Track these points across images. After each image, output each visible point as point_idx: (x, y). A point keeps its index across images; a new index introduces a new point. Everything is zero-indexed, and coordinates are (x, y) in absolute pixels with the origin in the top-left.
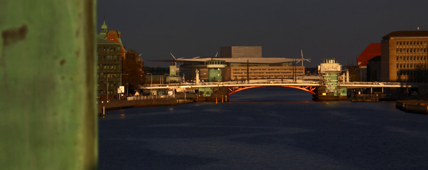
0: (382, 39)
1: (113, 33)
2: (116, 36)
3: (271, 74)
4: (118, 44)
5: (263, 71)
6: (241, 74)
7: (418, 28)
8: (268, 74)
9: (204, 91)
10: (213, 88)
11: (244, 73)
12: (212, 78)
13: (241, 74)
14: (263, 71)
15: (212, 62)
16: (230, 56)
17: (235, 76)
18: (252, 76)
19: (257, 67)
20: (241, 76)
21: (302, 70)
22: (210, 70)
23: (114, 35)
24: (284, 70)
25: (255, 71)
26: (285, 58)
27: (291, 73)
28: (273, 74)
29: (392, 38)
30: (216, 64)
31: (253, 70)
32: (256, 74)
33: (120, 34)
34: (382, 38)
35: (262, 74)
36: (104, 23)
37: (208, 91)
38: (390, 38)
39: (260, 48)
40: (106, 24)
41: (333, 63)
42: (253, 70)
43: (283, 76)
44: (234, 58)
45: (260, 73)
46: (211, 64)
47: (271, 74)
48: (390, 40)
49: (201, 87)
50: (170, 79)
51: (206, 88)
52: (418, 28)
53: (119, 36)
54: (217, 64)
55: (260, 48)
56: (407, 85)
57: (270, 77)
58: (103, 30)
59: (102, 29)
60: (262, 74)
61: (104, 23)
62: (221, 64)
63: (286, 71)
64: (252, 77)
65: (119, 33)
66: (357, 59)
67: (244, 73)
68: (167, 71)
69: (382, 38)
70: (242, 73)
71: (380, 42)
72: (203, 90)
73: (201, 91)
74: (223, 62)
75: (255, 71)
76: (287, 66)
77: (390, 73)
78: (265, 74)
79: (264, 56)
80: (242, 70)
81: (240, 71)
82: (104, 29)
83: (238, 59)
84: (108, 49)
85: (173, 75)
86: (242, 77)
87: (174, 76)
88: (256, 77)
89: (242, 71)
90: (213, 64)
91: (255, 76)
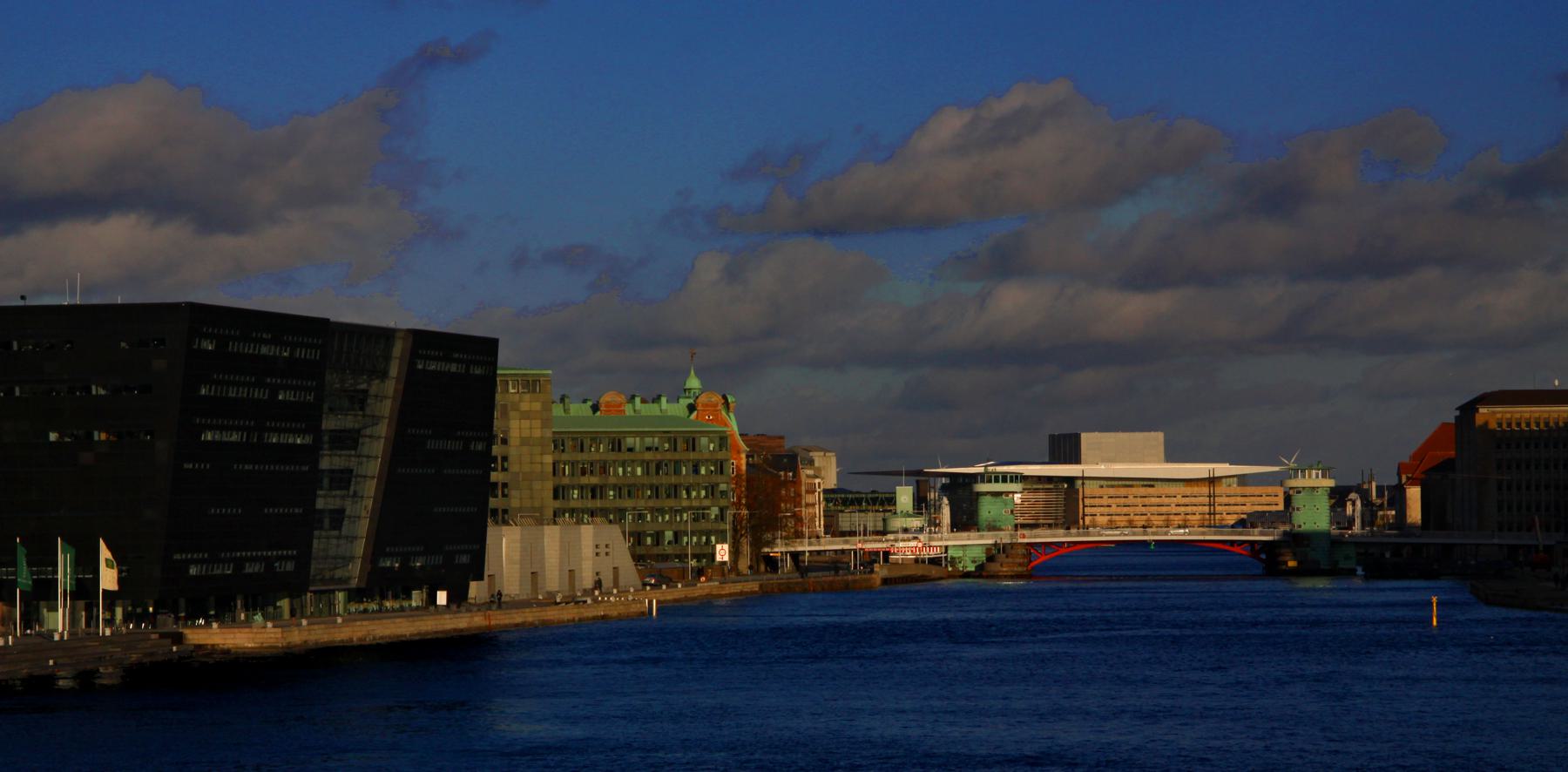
0: (1458, 413)
1: (713, 400)
2: (719, 408)
3: (1189, 509)
4: (725, 429)
5: (1167, 501)
6: (1106, 510)
7: (1557, 383)
8: (1182, 509)
9: (961, 555)
10: (988, 546)
11: (1114, 506)
12: (986, 521)
13: (1106, 510)
14: (1167, 501)
15: (988, 477)
16: (1075, 458)
17: (1091, 515)
18: (1137, 515)
19: (1150, 490)
20: (1108, 515)
21: (1277, 496)
22: (982, 497)
23: (716, 405)
24: (1227, 496)
25: (1146, 501)
26: (1230, 465)
27: (1245, 505)
28: (1194, 508)
29: (1483, 410)
30: (997, 480)
31: (1141, 497)
32: (1148, 508)
33: (732, 402)
34: (1457, 409)
35: (1164, 509)
36: (692, 372)
37: (975, 555)
38: (1478, 409)
39: (1160, 436)
40: (697, 374)
41: (1317, 477)
42: (1141, 497)
43: (1225, 513)
44: (1086, 463)
45: (1158, 506)
46: (983, 481)
47: (1189, 509)
48: (1477, 415)
49: (954, 546)
50: (897, 523)
51: (967, 548)
52: (1557, 383)
53: (731, 409)
54: (1006, 482)
55: (1160, 436)
56: (262, 555)
57: (1188, 517)
58: (689, 393)
59: (685, 390)
60: (1164, 509)
61: (692, 372)
62: (1011, 481)
63: (1232, 500)
64: (1137, 517)
65: (729, 400)
66: (1399, 468)
67: (1114, 506)
68: (892, 501)
69: (1457, 409)
70: (1110, 506)
71: (1452, 421)
72: (958, 554)
73: (954, 555)
74: (1017, 477)
75: (1146, 501)
76: (1235, 485)
77: (1408, 510)
78: (1175, 510)
79: (1172, 456)
80: (1183, 497)
81: (1105, 501)
82: (690, 389)
83: (1098, 467)
84: (601, 446)
85: (905, 511)
86: (1109, 517)
87: (908, 515)
88: (1148, 520)
89: (1110, 501)
90: (990, 481)
91: (1146, 515)
